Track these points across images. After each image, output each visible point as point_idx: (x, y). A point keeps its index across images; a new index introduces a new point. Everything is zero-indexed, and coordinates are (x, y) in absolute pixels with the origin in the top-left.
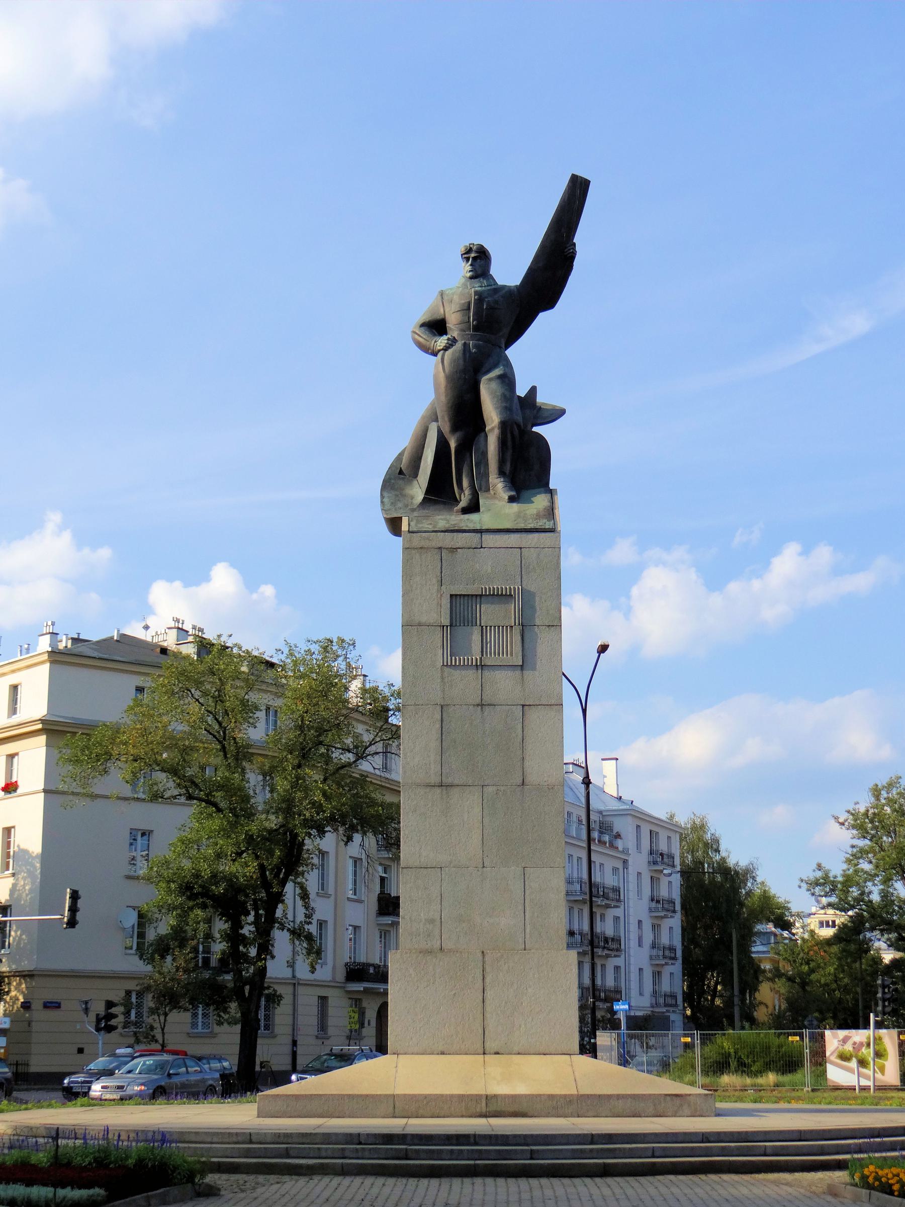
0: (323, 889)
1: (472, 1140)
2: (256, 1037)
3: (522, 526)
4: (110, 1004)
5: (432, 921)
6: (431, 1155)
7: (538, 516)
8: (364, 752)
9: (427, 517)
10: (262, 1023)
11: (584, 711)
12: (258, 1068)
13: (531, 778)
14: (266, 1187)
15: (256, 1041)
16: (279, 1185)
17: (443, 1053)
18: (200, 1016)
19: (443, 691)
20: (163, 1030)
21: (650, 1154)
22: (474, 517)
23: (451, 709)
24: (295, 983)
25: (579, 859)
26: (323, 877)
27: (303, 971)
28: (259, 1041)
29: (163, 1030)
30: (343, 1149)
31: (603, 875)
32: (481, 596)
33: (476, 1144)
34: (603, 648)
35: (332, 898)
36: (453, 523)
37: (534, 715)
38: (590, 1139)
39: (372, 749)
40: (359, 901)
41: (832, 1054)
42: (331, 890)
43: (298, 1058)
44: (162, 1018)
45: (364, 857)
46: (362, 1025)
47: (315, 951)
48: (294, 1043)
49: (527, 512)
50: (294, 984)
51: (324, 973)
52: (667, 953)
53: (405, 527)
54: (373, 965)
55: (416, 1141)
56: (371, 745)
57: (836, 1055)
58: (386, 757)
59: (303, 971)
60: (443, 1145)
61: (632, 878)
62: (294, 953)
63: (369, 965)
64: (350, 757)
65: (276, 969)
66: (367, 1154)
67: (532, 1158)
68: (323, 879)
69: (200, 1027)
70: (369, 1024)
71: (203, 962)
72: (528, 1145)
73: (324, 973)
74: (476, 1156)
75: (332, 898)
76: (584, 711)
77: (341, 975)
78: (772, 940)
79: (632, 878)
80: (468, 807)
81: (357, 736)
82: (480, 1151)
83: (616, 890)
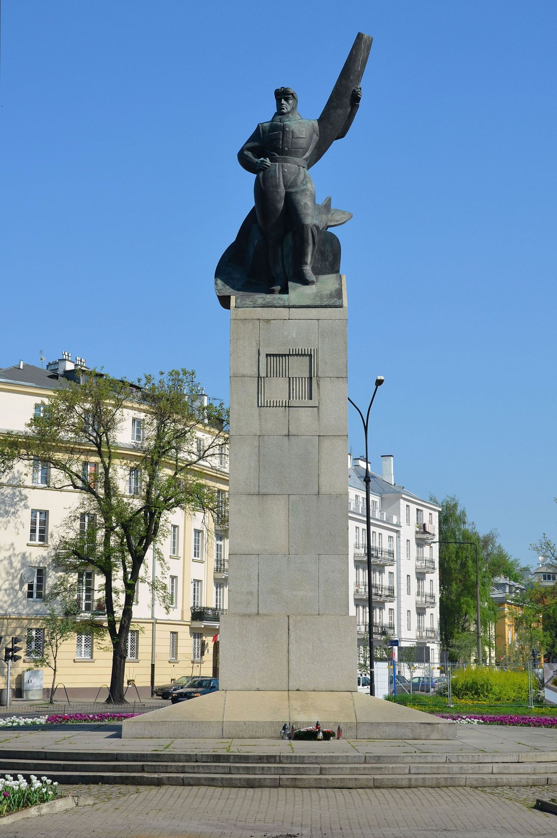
0: (174, 553)
1: (278, 759)
2: (125, 662)
3: (318, 303)
4: (15, 640)
5: (251, 593)
6: (248, 770)
7: (331, 296)
8: (204, 454)
9: (249, 297)
10: (129, 651)
11: (366, 428)
12: (125, 685)
13: (323, 490)
14: (126, 797)
15: (124, 665)
16: (136, 795)
17: (298, 690)
18: (83, 641)
19: (260, 425)
20: (55, 658)
21: (407, 771)
22: (285, 296)
23: (266, 438)
24: (154, 622)
25: (363, 530)
26: (174, 544)
27: (160, 613)
28: (126, 665)
29: (55, 658)
30: (184, 766)
31: (380, 542)
32: (288, 355)
33: (280, 762)
34: (379, 383)
35: (182, 559)
36: (268, 300)
37: (326, 443)
38: (363, 759)
39: (210, 452)
40: (202, 562)
41: (548, 681)
42: (181, 554)
43: (155, 669)
44: (54, 648)
45: (205, 530)
46: (202, 654)
47: (170, 601)
48: (153, 666)
49: (323, 293)
50: (153, 623)
51: (175, 615)
52: (428, 599)
53: (233, 303)
54: (211, 609)
55: (237, 760)
56: (209, 448)
57: (551, 681)
58: (221, 458)
59: (160, 613)
60: (257, 763)
61: (403, 544)
62: (153, 599)
63: (208, 609)
64: (195, 458)
65: (139, 611)
66: (201, 770)
67: (321, 774)
68: (174, 545)
69: (83, 655)
70: (208, 652)
71: (86, 607)
72: (318, 763)
73: (175, 615)
74: (281, 772)
75: (182, 559)
76: (366, 428)
77: (188, 616)
78: (507, 590)
79: (403, 544)
80: (277, 510)
81: (199, 441)
82: (284, 768)
83: (391, 553)
